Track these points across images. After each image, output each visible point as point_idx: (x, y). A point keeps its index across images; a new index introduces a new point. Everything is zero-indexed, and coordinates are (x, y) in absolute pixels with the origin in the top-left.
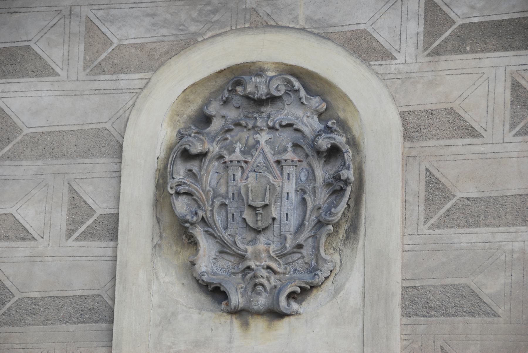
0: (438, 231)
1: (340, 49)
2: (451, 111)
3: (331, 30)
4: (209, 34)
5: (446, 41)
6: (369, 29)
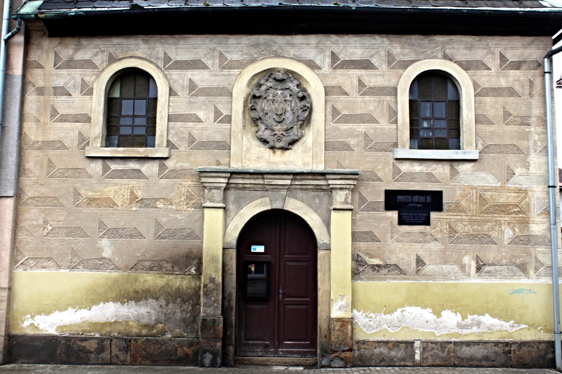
0: (336, 124)
1: (305, 65)
2: (340, 87)
3: (301, 59)
4: (261, 58)
5: (338, 65)
6: (314, 60)
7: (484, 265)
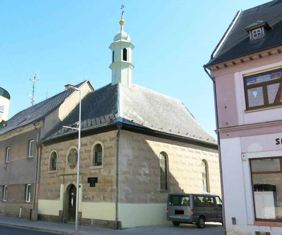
7: (105, 198)
